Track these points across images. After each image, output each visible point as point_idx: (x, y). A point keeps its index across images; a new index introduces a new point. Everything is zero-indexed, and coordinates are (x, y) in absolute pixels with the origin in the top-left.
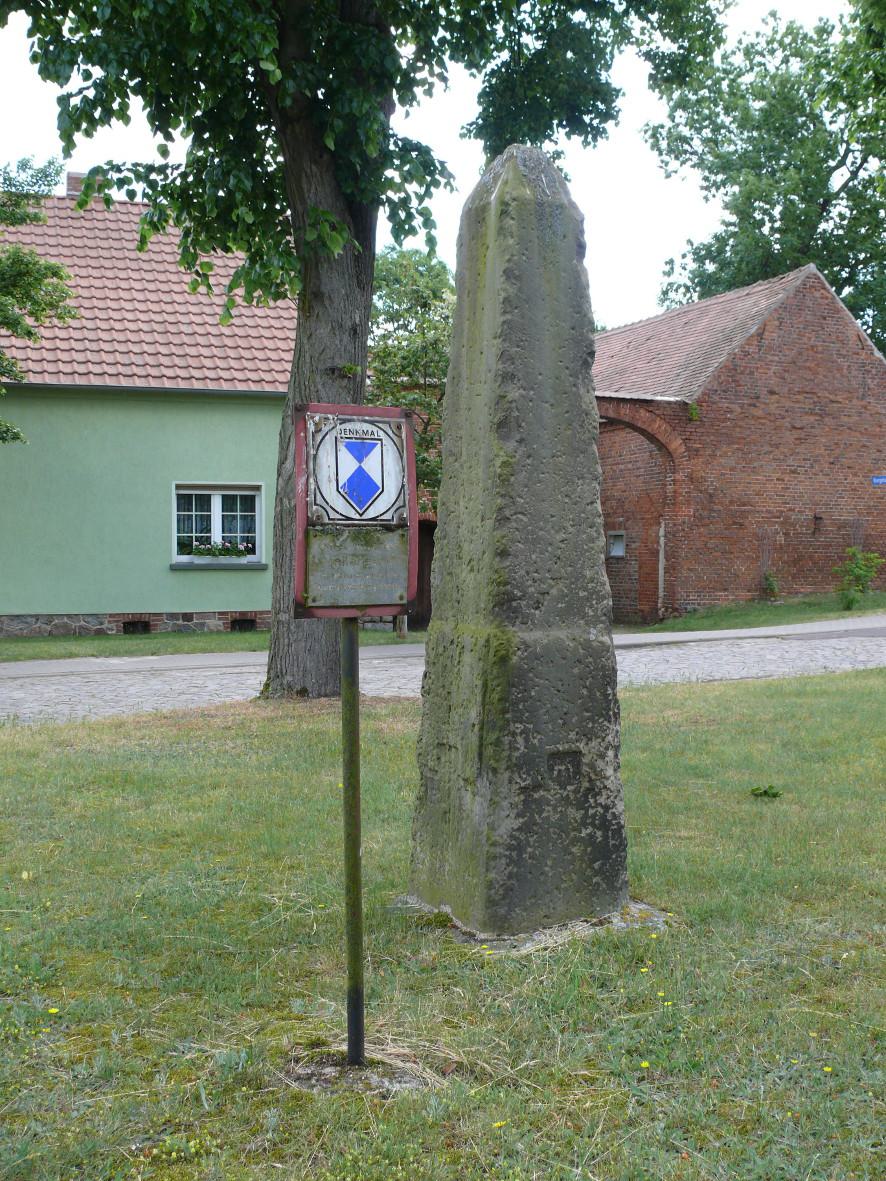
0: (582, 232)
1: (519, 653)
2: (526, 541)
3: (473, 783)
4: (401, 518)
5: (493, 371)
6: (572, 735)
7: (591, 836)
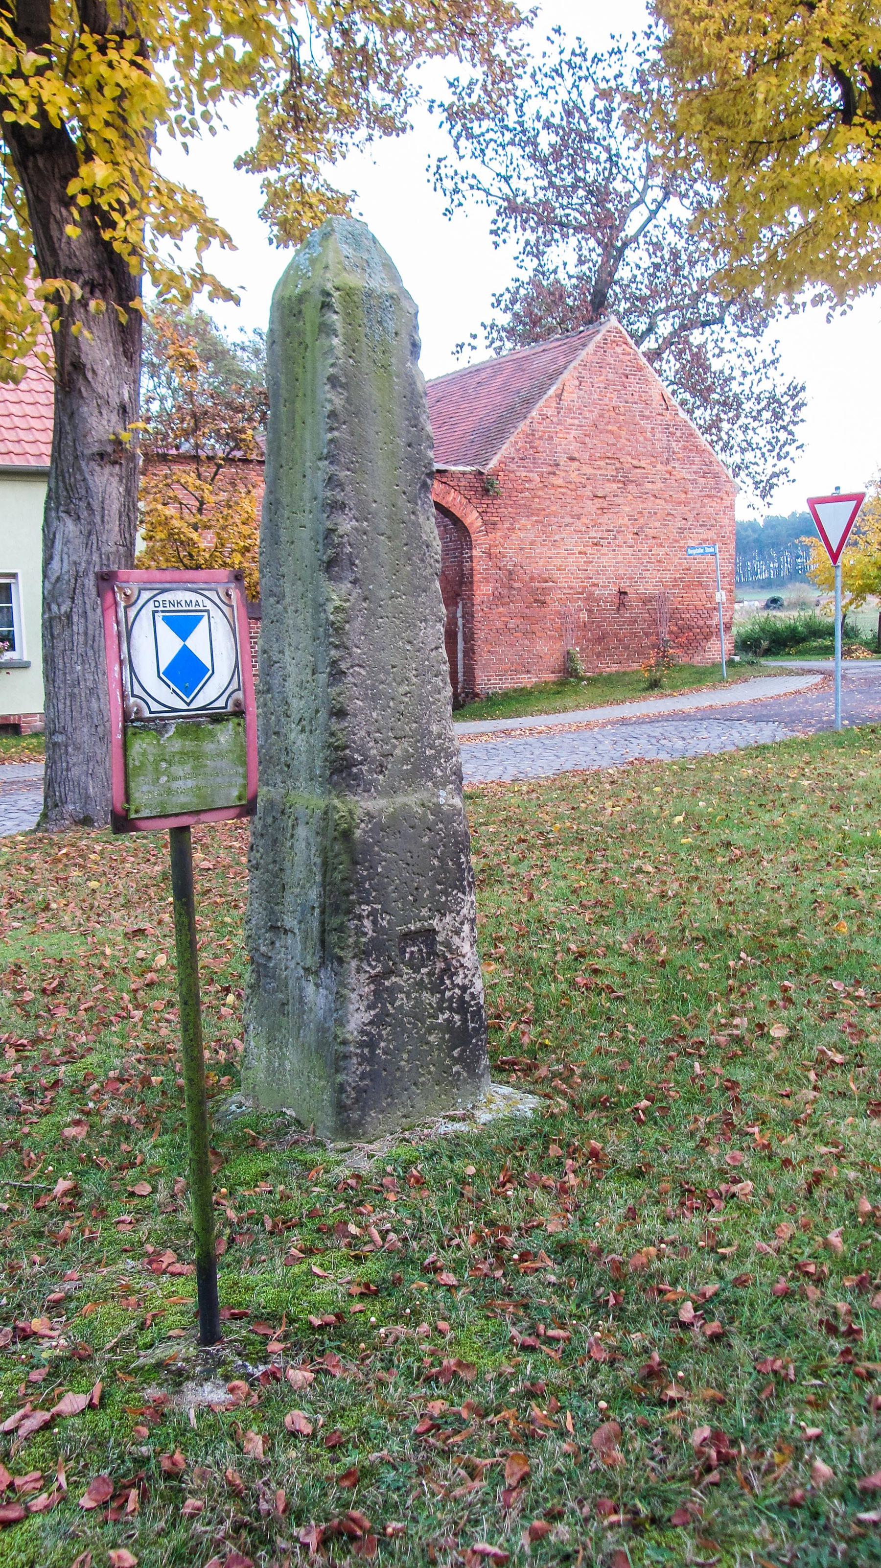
0: (416, 327)
1: (363, 825)
2: (365, 698)
3: (316, 973)
4: (237, 704)
5: (320, 500)
6: (424, 912)
7: (448, 1021)
